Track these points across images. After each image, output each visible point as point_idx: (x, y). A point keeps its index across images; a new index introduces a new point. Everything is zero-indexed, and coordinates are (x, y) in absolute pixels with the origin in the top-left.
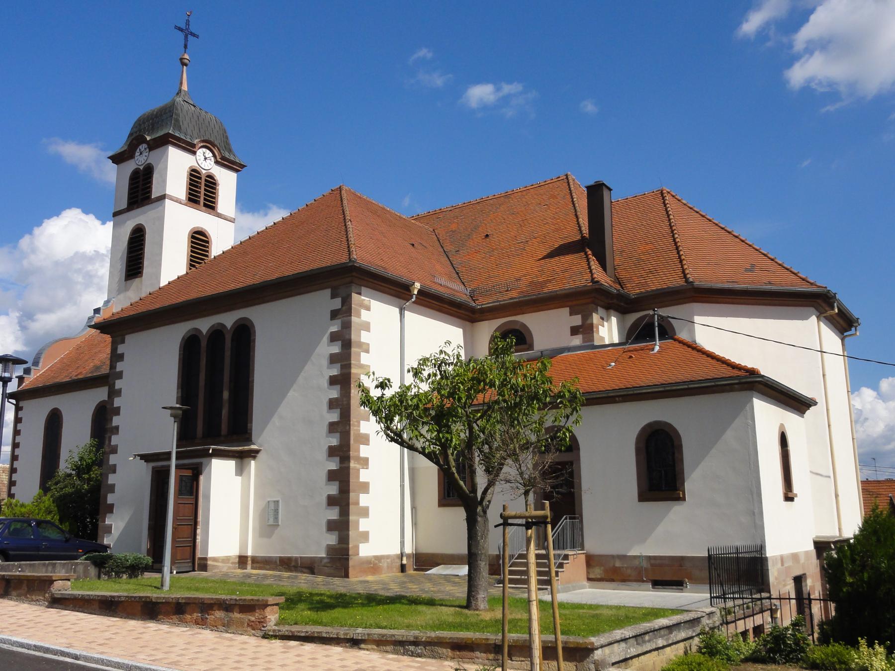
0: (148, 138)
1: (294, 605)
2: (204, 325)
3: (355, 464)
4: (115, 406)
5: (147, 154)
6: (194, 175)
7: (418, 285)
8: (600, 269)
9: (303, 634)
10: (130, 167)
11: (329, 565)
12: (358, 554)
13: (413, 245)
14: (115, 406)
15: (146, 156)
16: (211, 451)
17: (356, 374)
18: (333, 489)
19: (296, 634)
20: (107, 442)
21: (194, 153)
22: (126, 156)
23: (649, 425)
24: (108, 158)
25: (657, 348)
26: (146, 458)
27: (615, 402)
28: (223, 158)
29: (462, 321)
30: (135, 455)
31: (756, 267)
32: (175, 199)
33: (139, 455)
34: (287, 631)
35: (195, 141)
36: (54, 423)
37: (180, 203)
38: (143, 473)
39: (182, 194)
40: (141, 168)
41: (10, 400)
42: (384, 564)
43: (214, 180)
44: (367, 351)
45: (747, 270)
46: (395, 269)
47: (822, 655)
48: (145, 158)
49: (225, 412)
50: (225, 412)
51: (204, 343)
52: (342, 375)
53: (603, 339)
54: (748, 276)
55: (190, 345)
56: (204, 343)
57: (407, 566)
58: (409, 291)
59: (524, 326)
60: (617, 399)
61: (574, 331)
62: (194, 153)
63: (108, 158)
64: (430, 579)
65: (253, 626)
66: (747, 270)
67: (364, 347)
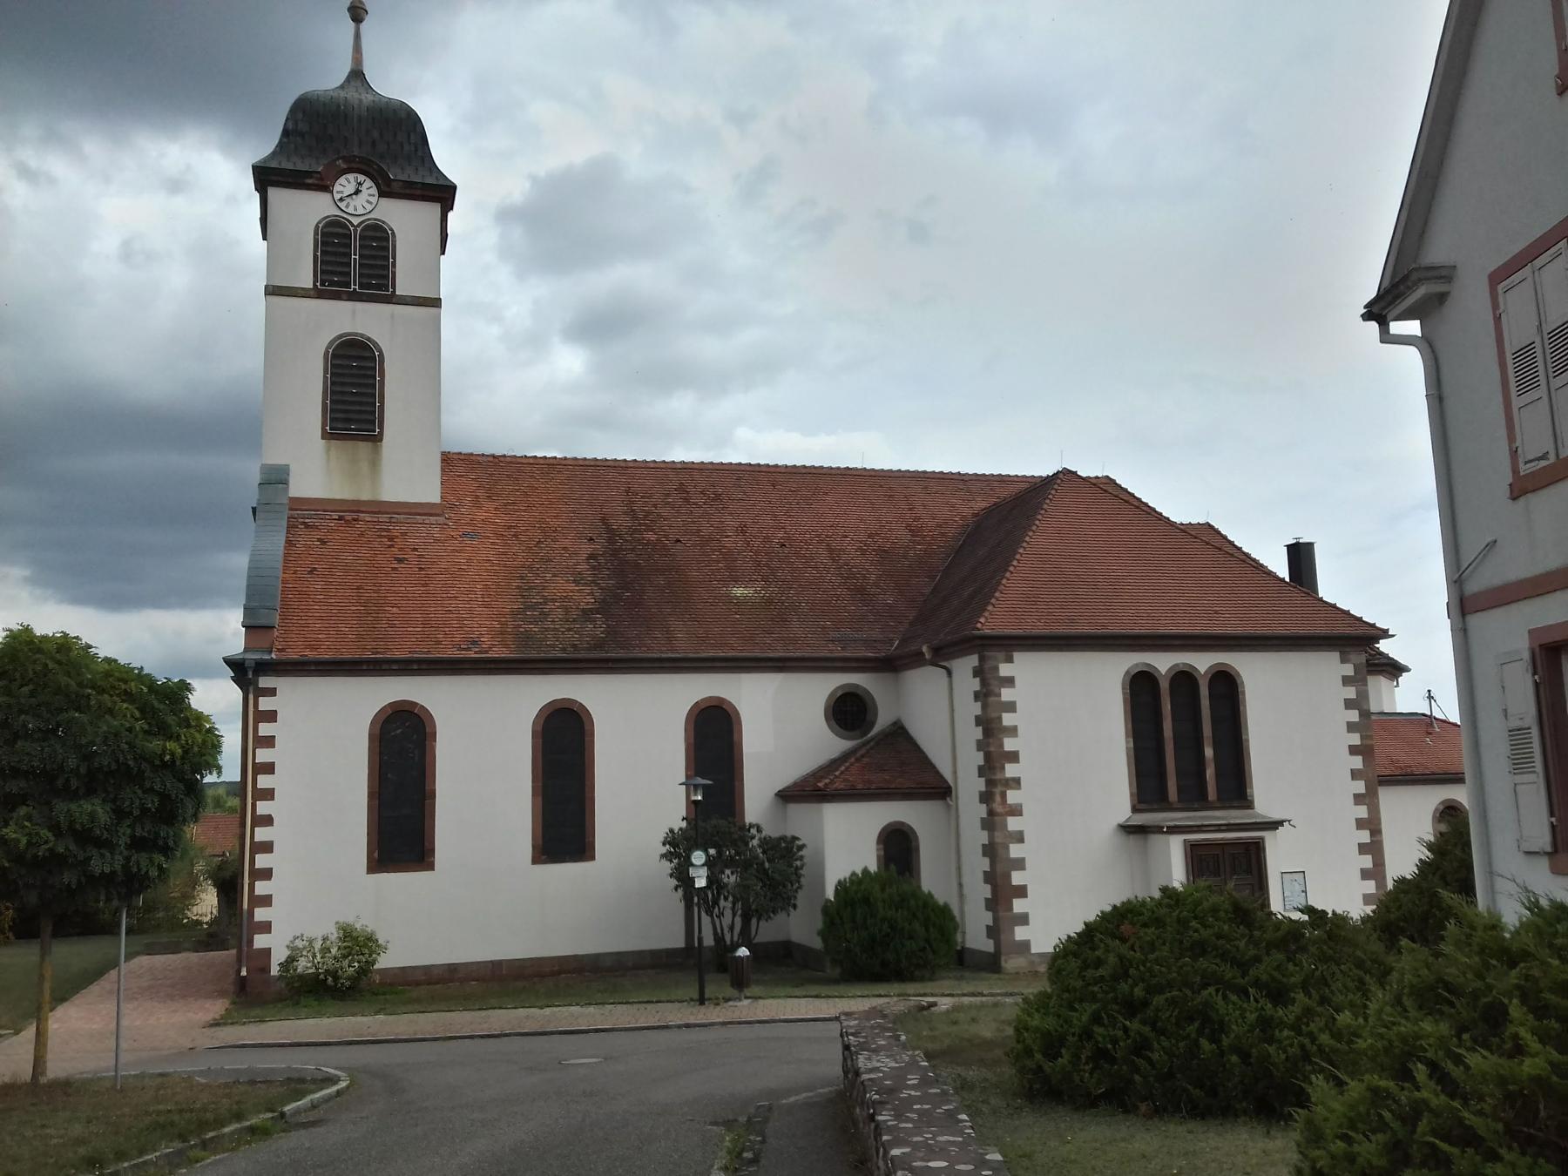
2: (1163, 663)
16: (1165, 830)
50: (1210, 773)
56: (1164, 685)
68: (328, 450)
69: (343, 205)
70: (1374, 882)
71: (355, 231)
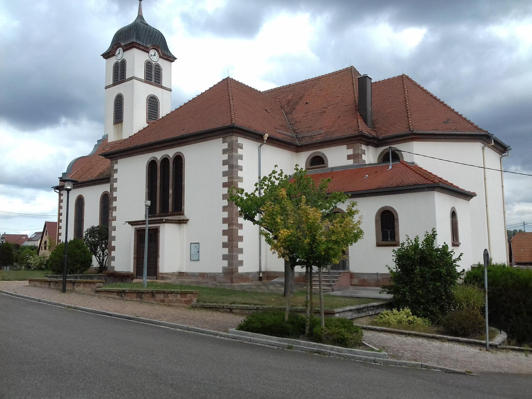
0: (123, 44)
1: (11, 250)
2: (159, 155)
3: (235, 227)
4: (114, 196)
5: (122, 53)
6: (148, 65)
7: (267, 135)
8: (364, 124)
9: (208, 306)
10: (113, 60)
11: (223, 277)
12: (238, 272)
13: (266, 110)
14: (114, 196)
15: (121, 55)
16: (164, 221)
17: (235, 182)
18: (225, 239)
19: (205, 306)
20: (110, 214)
21: (148, 52)
22: (110, 54)
23: (383, 208)
24: (101, 55)
25: (390, 167)
26: (132, 223)
27: (365, 196)
28: (164, 55)
29: (292, 152)
30: (126, 222)
31: (450, 120)
32: (139, 79)
33: (128, 222)
34: (201, 305)
35: (148, 46)
36: (80, 202)
37: (142, 81)
38: (131, 231)
39: (142, 76)
40: (119, 61)
41: (56, 190)
42: (345, 256)
43: (160, 67)
44: (241, 170)
45: (444, 122)
46: (255, 126)
47: (309, 303)
48: (121, 56)
49: (170, 200)
50: (170, 200)
51: (159, 165)
52: (228, 182)
53: (364, 161)
54: (444, 125)
55: (152, 165)
56: (159, 165)
57: (262, 278)
58: (263, 138)
59: (323, 154)
60: (366, 195)
61: (349, 157)
62: (148, 52)
63: (101, 55)
64: (272, 284)
65: (186, 302)
66: (444, 122)
67: (240, 168)
68: (114, 127)
69: (151, 58)
70: (112, 251)
71: (154, 66)
